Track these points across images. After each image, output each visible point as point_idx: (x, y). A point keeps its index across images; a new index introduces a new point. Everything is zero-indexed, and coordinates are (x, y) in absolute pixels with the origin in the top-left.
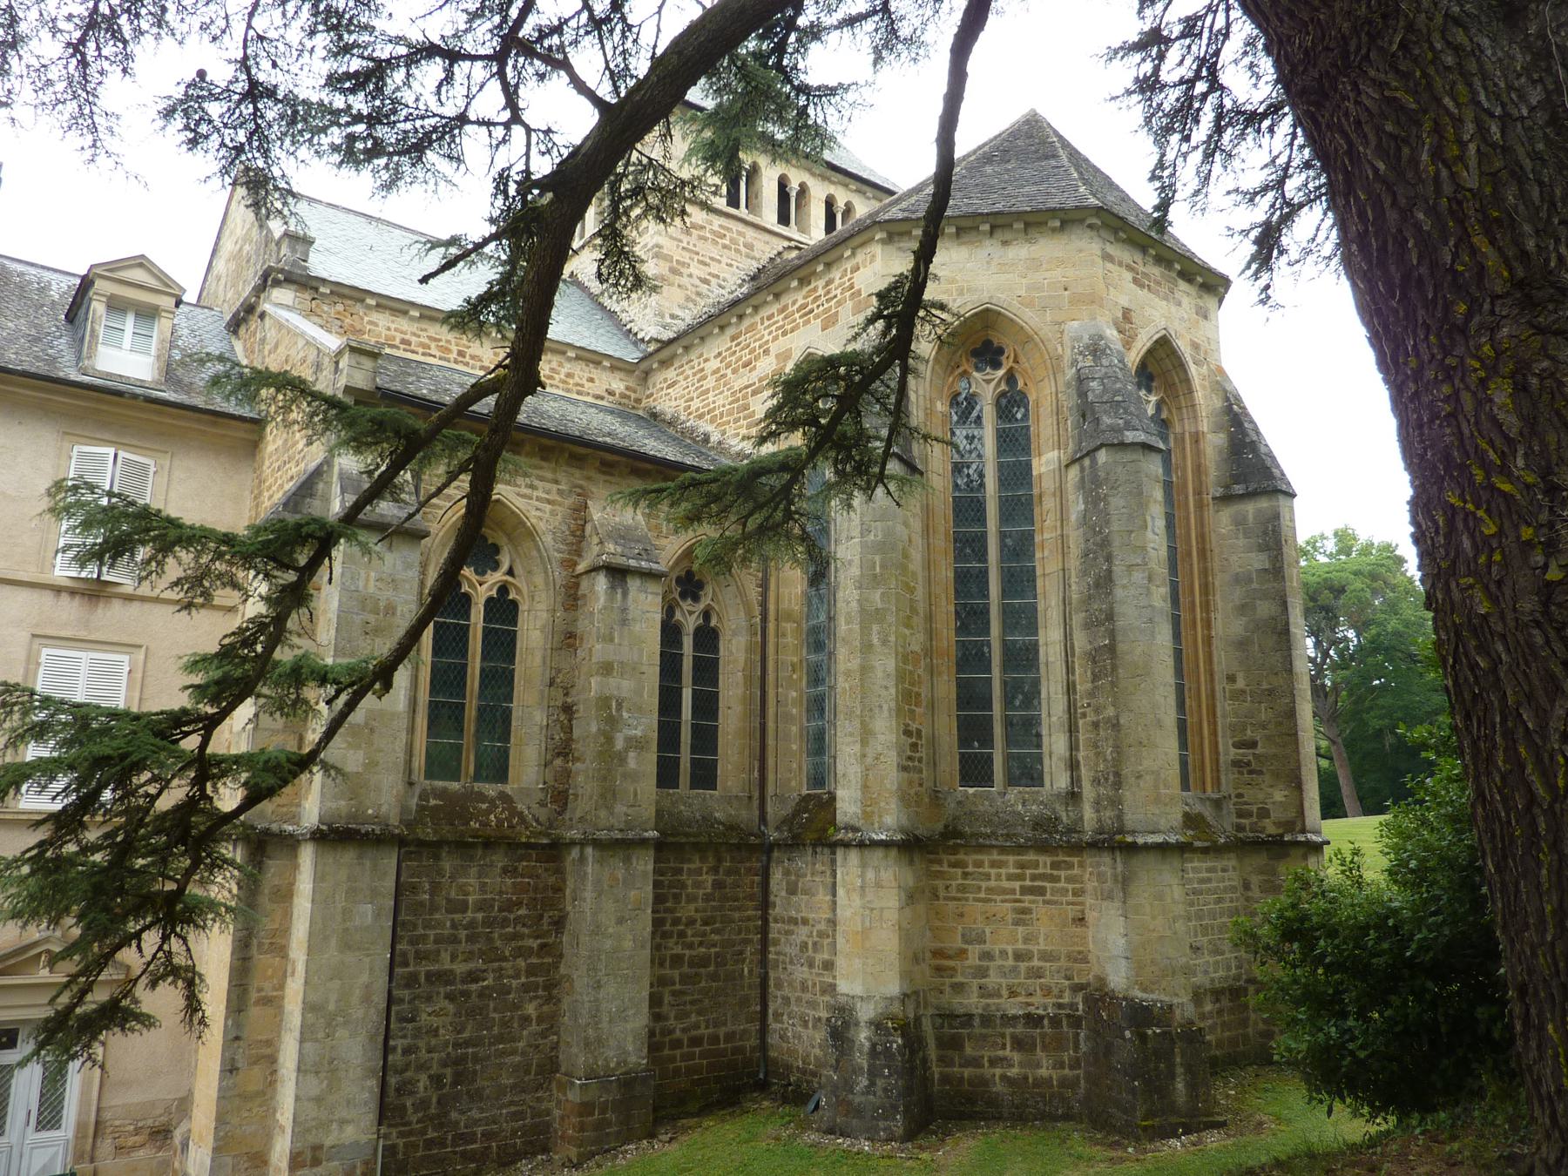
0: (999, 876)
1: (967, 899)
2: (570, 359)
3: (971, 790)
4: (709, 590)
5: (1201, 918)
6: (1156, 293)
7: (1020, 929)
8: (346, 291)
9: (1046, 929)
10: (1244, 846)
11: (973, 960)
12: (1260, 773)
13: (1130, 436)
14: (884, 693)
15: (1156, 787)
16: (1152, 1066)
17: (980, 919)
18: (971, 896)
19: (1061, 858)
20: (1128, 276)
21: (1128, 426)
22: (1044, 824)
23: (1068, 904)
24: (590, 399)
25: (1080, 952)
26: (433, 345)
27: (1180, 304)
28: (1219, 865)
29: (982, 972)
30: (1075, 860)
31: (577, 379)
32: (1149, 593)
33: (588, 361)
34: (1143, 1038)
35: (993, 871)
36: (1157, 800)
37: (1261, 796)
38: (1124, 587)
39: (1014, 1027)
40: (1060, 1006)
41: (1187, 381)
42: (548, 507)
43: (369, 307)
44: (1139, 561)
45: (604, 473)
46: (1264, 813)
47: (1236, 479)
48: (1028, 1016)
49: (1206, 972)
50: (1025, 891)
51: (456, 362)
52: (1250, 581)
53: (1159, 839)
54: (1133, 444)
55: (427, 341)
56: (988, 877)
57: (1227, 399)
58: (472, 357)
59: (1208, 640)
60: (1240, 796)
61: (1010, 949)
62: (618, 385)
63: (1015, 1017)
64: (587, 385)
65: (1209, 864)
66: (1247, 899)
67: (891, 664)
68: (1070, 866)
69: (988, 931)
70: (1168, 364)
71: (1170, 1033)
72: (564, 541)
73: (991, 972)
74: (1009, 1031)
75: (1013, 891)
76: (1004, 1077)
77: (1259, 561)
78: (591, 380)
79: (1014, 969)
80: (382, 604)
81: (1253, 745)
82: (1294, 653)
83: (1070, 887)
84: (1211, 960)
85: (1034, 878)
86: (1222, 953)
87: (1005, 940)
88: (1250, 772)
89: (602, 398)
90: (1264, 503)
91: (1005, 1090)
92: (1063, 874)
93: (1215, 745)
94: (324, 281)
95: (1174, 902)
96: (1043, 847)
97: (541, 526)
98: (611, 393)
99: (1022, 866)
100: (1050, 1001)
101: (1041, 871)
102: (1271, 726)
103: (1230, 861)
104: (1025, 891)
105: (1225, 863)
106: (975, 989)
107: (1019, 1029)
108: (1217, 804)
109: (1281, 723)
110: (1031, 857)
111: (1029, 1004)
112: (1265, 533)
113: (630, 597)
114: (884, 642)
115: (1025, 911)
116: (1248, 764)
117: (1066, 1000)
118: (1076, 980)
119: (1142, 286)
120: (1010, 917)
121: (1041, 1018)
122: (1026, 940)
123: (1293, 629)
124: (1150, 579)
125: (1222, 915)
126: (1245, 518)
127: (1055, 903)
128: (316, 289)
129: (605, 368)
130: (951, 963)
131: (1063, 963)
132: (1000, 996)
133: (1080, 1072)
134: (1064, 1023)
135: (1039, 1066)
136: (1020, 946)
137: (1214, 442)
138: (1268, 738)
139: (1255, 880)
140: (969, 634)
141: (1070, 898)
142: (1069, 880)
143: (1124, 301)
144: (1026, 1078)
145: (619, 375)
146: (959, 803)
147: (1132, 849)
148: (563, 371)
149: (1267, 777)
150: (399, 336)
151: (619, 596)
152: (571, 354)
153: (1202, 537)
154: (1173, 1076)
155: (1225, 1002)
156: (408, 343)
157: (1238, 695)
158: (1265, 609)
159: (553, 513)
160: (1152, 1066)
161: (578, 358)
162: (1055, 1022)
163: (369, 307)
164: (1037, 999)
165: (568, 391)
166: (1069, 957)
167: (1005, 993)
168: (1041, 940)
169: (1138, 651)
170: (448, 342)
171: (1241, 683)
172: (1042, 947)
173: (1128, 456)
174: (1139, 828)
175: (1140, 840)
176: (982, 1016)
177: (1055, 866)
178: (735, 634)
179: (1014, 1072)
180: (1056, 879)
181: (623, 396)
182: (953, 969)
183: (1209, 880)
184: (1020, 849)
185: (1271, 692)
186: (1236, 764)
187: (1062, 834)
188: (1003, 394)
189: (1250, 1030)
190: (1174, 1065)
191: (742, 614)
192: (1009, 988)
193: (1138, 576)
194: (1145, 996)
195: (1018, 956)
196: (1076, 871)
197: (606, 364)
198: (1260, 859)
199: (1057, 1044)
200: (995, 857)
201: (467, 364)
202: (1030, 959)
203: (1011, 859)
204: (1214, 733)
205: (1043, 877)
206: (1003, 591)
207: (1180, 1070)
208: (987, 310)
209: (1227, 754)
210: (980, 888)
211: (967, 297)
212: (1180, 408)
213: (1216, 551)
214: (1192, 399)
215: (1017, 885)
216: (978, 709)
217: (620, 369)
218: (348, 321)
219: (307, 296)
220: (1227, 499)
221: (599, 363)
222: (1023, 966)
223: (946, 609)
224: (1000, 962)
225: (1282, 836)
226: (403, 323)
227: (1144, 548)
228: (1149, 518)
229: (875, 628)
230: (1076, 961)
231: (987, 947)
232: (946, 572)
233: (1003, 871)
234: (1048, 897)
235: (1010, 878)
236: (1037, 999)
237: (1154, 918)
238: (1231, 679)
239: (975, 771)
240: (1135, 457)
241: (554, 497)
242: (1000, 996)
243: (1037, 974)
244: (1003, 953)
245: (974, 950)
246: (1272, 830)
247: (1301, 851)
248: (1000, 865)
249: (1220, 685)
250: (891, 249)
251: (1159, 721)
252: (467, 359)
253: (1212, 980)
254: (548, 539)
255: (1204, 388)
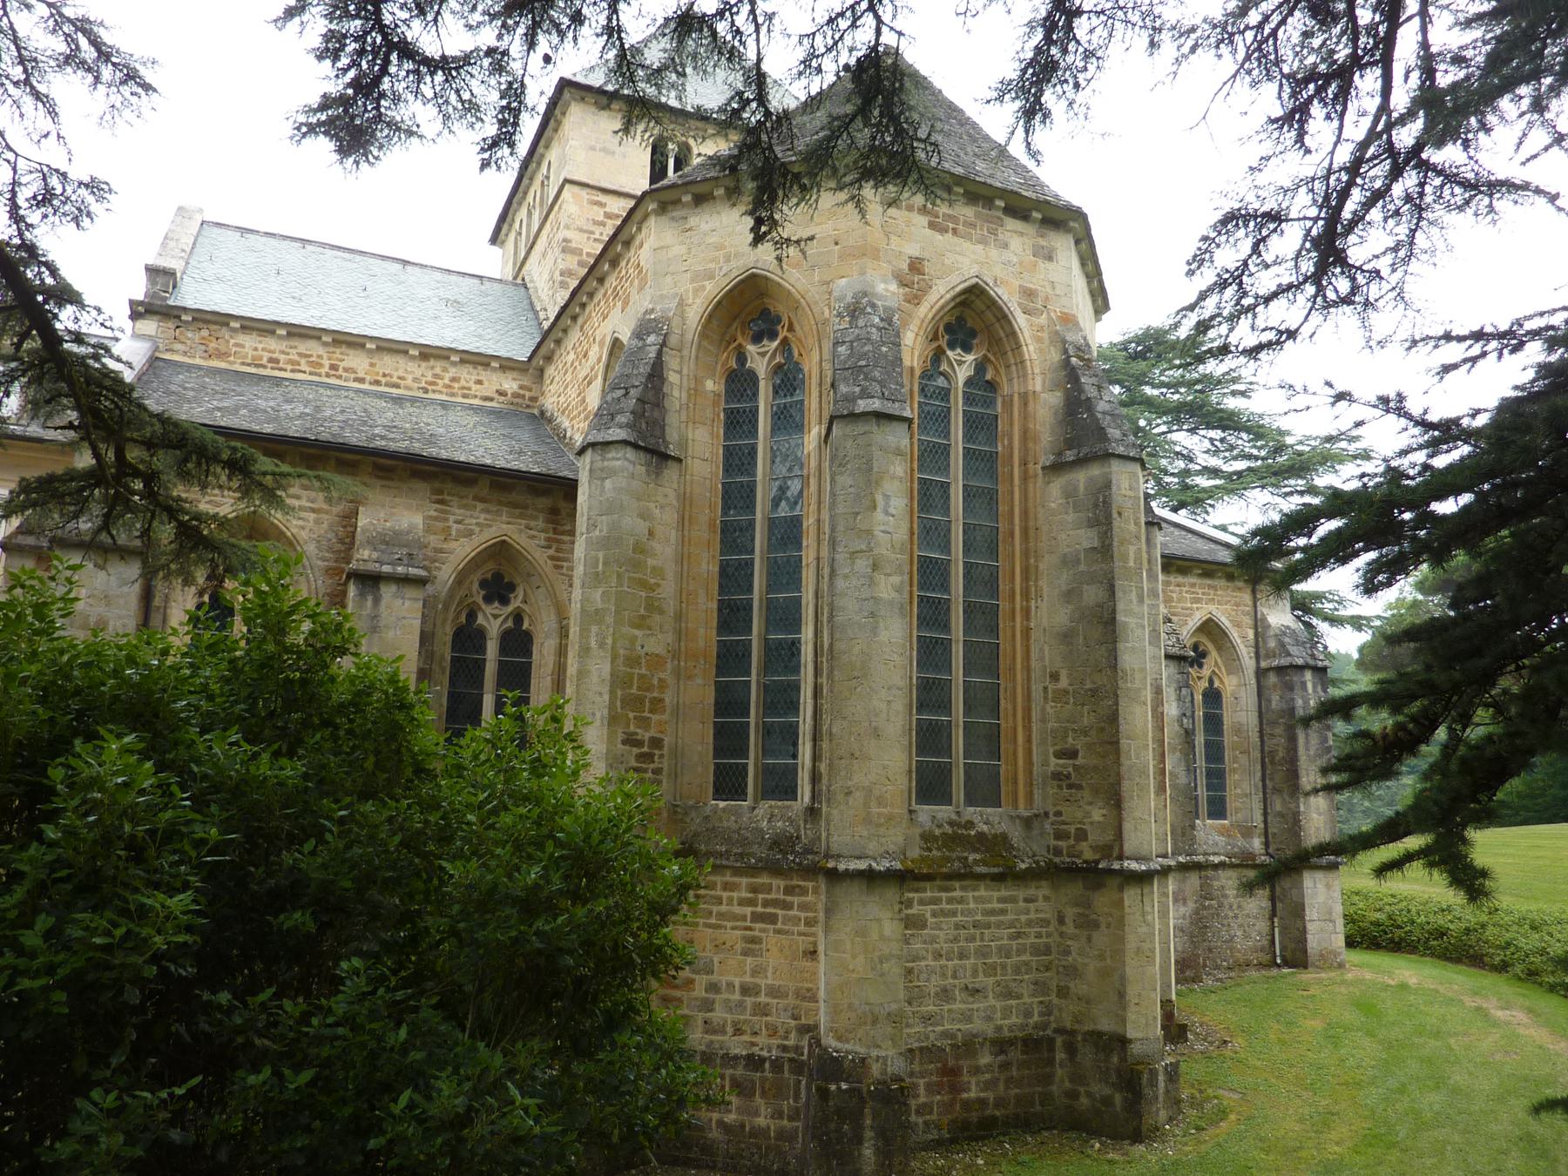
0: (730, 900)
1: (697, 924)
2: (454, 364)
3: (722, 804)
4: (520, 592)
5: (984, 956)
6: (968, 237)
7: (749, 960)
8: (209, 317)
9: (775, 962)
10: (1054, 872)
11: (699, 992)
12: (1080, 787)
13: (862, 405)
14: (598, 699)
15: (866, 805)
16: (832, 1126)
17: (709, 947)
18: (701, 921)
19: (795, 882)
20: (923, 220)
21: (865, 394)
22: (784, 843)
23: (800, 934)
24: (476, 402)
25: (809, 990)
26: (303, 361)
27: (1006, 246)
28: (1021, 894)
29: (708, 1006)
30: (810, 885)
31: (463, 383)
32: (872, 583)
33: (475, 364)
34: (824, 1094)
35: (725, 895)
36: (867, 820)
37: (1079, 815)
38: (846, 577)
39: (734, 1067)
40: (784, 1048)
41: (1013, 334)
42: (312, 516)
43: (234, 330)
44: (863, 547)
45: (378, 477)
46: (1082, 835)
47: (1070, 444)
48: (750, 1057)
49: (989, 1019)
50: (757, 918)
51: (328, 375)
52: (1078, 562)
53: (862, 865)
54: (865, 414)
55: (296, 358)
56: (719, 901)
57: (1066, 351)
58: (346, 370)
59: (1027, 632)
60: (1058, 814)
61: (737, 982)
62: (510, 384)
63: (736, 1058)
64: (475, 387)
65: (1004, 893)
66: (1062, 935)
67: (607, 668)
68: (804, 892)
69: (716, 960)
70: (989, 316)
71: (859, 1091)
72: (330, 549)
73: (717, 1006)
74: (729, 1072)
75: (744, 918)
76: (720, 1123)
77: (1087, 538)
78: (480, 382)
79: (741, 1004)
80: (92, 621)
81: (1073, 754)
82: (1121, 646)
83: (803, 915)
84: (998, 1005)
85: (766, 904)
86: (1019, 997)
87: (732, 971)
88: (1070, 787)
89: (492, 399)
90: (1095, 471)
91: (721, 1137)
92: (796, 900)
93: (1029, 752)
94: (185, 309)
95: (882, 937)
96: (776, 870)
97: (304, 535)
98: (501, 393)
99: (754, 889)
100: (775, 1042)
101: (773, 896)
102: (1093, 733)
103: (1042, 890)
104: (757, 918)
105: (1031, 892)
106: (700, 1022)
107: (740, 1071)
108: (1028, 823)
109: (1103, 729)
110: (764, 880)
111: (753, 1044)
112: (1096, 506)
113: (383, 603)
114: (602, 645)
115: (753, 940)
116: (1068, 777)
117: (791, 1042)
118: (803, 1021)
119: (943, 230)
120: (739, 946)
121: (762, 1060)
122: (755, 973)
123: (1121, 617)
124: (875, 567)
125: (1020, 952)
126: (1076, 489)
127: (787, 933)
128: (179, 317)
129: (494, 369)
130: (678, 993)
131: (791, 1000)
132: (724, 1032)
133: (799, 1124)
134: (786, 1067)
135: (757, 1114)
136: (748, 979)
137: (1047, 403)
138: (1089, 747)
139: (1070, 912)
140: (731, 633)
141: (802, 928)
142: (804, 907)
143: (913, 250)
144: (743, 1126)
145: (510, 375)
146: (707, 818)
147: (834, 876)
148: (447, 376)
149: (1086, 793)
150: (266, 355)
151: (369, 603)
152: (455, 358)
153: (1025, 513)
154: (859, 1140)
155: (1015, 1054)
156: (277, 361)
157: (1061, 695)
158: (1092, 594)
159: (317, 522)
160: (832, 1126)
161: (462, 361)
162: (777, 1065)
163: (234, 330)
164: (762, 1040)
165: (453, 395)
166: (797, 994)
167: (730, 1030)
168: (769, 974)
169: (856, 650)
170: (319, 357)
171: (1064, 683)
172: (770, 982)
173: (861, 428)
174: (845, 852)
175: (842, 867)
176: (703, 1053)
177: (789, 890)
178: (547, 637)
179: (731, 1118)
180: (787, 906)
181: (516, 395)
182: (680, 1000)
183: (1003, 912)
184: (752, 871)
185: (1094, 692)
186: (1057, 776)
187: (797, 854)
188: (779, 367)
189: (1054, 1088)
190: (862, 1128)
191: (553, 617)
192: (735, 1024)
193: (862, 564)
194: (839, 1045)
195: (746, 990)
196: (810, 898)
197: (495, 364)
198: (1075, 889)
199: (776, 1091)
200: (728, 878)
201: (340, 377)
202: (757, 994)
203: (744, 881)
204: (1029, 741)
205: (775, 903)
206: (769, 586)
207: (869, 1134)
208: (754, 276)
209: (1045, 763)
210: (711, 913)
211: (733, 264)
212: (1008, 366)
213: (1045, 529)
214: (1021, 355)
215: (748, 910)
216: (736, 716)
217: (513, 369)
218: (213, 345)
219: (171, 324)
220: (1057, 468)
221: (488, 365)
222: (749, 1000)
223: (706, 607)
224: (725, 996)
225: (1097, 862)
226: (271, 343)
227: (869, 532)
228: (879, 498)
229: (594, 629)
230: (804, 999)
231: (714, 978)
232: (708, 565)
233: (735, 894)
234: (779, 925)
235: (742, 902)
236: (762, 1040)
237: (854, 957)
238: (1055, 677)
239: (729, 784)
240: (867, 428)
241: (321, 504)
242: (724, 1032)
243: (762, 1010)
244: (730, 985)
245: (701, 980)
246: (1089, 855)
247: (1116, 881)
248: (727, 887)
249: (1036, 689)
250: (664, 219)
251: (876, 729)
252: (340, 372)
253: (999, 1029)
254: (311, 549)
255: (1039, 340)
